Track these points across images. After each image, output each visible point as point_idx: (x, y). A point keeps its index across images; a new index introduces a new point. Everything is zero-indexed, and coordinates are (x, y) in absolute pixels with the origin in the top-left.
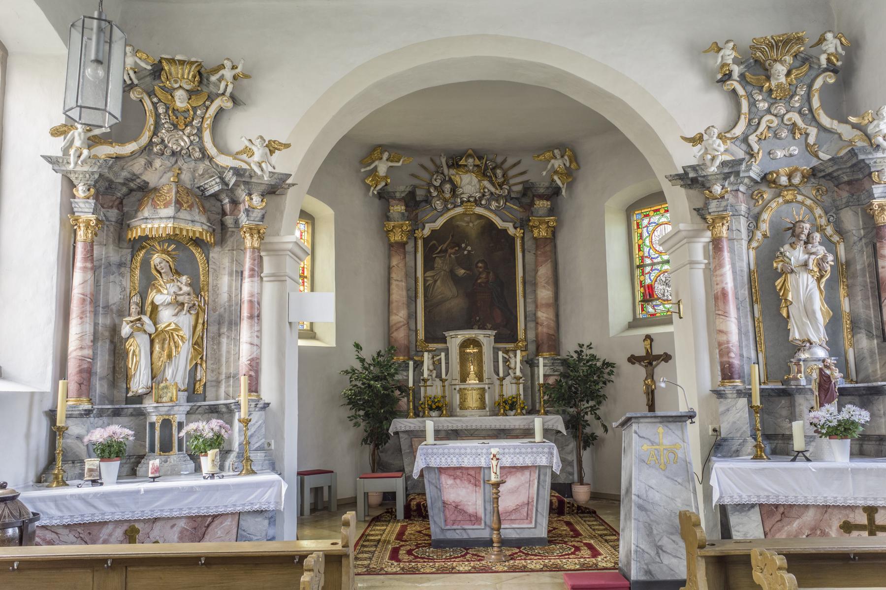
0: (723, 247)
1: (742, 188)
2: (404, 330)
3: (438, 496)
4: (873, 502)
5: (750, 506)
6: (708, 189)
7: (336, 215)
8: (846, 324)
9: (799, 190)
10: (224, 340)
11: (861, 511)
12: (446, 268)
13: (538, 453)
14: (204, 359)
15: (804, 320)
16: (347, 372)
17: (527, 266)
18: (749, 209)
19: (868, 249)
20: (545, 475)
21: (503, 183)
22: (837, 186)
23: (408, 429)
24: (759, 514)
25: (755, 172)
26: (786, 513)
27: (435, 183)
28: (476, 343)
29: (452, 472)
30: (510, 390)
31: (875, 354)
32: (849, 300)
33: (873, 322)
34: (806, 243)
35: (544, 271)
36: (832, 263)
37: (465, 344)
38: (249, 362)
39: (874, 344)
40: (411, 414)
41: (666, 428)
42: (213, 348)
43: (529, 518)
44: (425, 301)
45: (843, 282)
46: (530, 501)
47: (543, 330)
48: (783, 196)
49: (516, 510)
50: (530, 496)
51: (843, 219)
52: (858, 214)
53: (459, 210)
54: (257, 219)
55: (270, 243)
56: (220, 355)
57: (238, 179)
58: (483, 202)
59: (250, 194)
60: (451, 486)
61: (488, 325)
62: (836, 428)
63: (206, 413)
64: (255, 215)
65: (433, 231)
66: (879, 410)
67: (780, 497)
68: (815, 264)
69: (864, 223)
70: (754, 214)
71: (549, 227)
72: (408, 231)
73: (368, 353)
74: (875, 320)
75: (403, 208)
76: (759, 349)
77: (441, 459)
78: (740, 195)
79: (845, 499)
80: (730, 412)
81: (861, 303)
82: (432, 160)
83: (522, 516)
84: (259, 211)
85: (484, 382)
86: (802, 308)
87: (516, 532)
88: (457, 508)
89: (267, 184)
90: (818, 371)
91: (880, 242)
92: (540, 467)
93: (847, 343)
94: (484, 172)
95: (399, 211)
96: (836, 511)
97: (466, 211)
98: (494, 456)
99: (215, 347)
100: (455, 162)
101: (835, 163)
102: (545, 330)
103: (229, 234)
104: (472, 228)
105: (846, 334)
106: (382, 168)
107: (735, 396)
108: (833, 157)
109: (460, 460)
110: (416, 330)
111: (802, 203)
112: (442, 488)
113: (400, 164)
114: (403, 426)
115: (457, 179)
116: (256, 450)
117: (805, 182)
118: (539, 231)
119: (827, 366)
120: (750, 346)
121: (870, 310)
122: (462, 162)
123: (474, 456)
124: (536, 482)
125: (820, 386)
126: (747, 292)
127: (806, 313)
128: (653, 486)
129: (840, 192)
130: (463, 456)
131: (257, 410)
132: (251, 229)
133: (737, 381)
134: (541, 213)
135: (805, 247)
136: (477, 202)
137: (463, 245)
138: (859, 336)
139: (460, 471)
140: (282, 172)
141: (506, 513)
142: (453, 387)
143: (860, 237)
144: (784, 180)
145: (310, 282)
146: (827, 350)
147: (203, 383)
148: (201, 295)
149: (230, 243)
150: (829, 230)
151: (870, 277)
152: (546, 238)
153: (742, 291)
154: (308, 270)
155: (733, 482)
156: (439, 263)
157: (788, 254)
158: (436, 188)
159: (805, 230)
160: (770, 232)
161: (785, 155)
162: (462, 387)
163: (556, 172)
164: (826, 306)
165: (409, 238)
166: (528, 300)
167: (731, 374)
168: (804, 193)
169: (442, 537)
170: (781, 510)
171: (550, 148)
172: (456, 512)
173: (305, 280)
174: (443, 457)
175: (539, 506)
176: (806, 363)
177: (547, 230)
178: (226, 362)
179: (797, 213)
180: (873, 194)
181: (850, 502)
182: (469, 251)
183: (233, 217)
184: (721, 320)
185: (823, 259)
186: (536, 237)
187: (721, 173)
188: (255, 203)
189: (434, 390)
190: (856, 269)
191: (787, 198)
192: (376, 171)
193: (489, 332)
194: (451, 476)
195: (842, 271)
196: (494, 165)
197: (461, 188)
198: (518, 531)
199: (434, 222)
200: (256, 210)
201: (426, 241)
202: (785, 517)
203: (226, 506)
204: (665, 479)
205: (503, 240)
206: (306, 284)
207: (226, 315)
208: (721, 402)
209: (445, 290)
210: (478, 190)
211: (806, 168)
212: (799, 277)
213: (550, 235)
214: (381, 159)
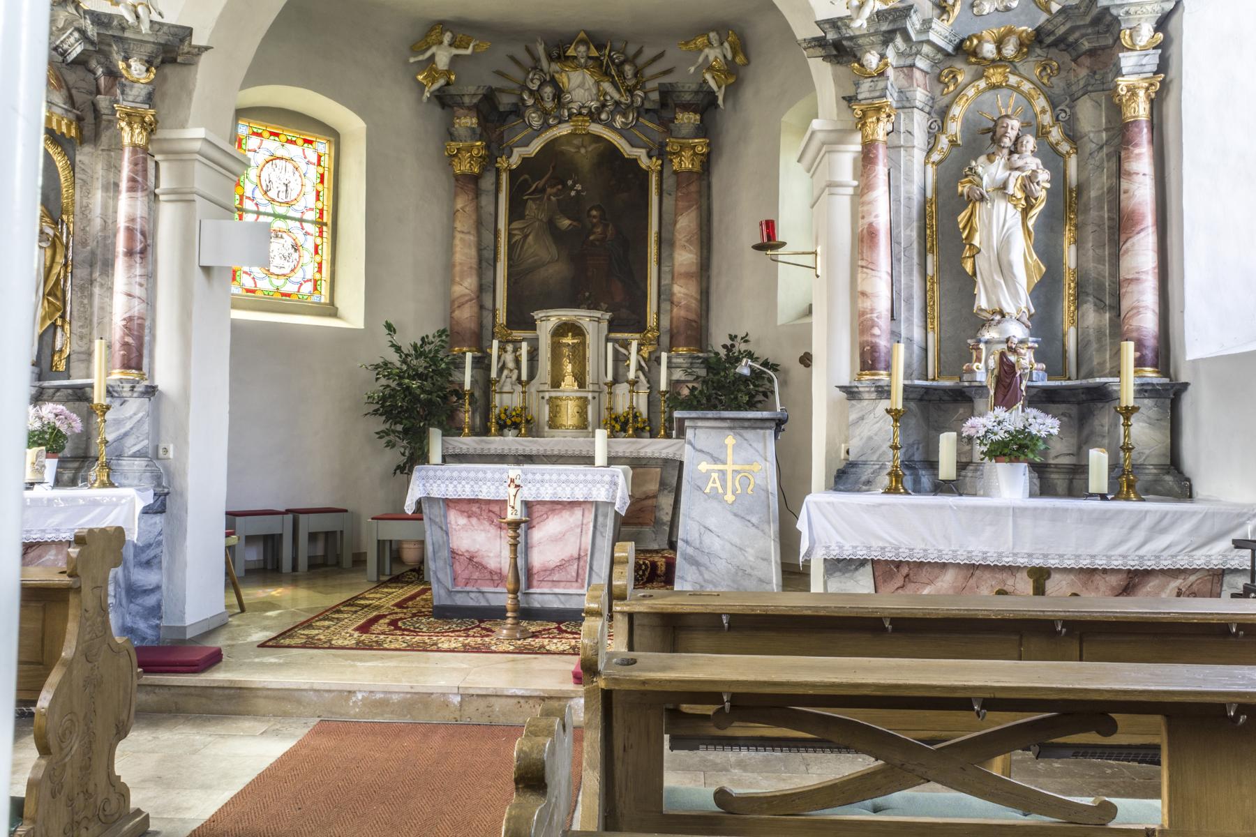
0: (876, 157)
1: (921, 63)
2: (471, 307)
3: (444, 542)
4: (1042, 561)
5: (857, 564)
6: (859, 61)
7: (368, 130)
8: (1069, 288)
9: (1015, 67)
10: (97, 290)
11: (1025, 574)
12: (542, 216)
13: (594, 482)
14: (68, 318)
15: (996, 277)
16: (377, 367)
17: (665, 216)
18: (933, 99)
19: (1110, 164)
20: (606, 516)
21: (635, 87)
22: (1075, 60)
23: (457, 451)
24: (872, 576)
25: (941, 33)
26: (911, 575)
27: (531, 86)
28: (577, 330)
29: (465, 507)
30: (623, 401)
31: (1106, 335)
32: (1078, 250)
33: (1107, 284)
34: (1011, 153)
35: (686, 223)
36: (1048, 185)
37: (562, 330)
38: (124, 323)
39: (1106, 320)
40: (466, 430)
41: (738, 437)
42: (82, 303)
43: (579, 580)
44: (509, 267)
45: (1070, 219)
46: (582, 554)
47: (679, 313)
48: (987, 77)
49: (561, 567)
50: (583, 547)
51: (1080, 116)
52: (1100, 106)
53: (565, 130)
54: (139, 99)
55: (165, 140)
56: (92, 314)
57: (101, 32)
58: (603, 116)
59: (126, 59)
60: (464, 527)
61: (602, 304)
62: (1003, 444)
63: (69, 401)
64: (135, 92)
65: (525, 161)
66: (1102, 426)
67: (900, 550)
68: (1018, 185)
69: (1109, 121)
70: (941, 108)
71: (695, 154)
72: (480, 157)
73: (408, 339)
74: (1110, 281)
75: (474, 120)
76: (929, 326)
77: (447, 486)
78: (917, 74)
79: (1000, 555)
80: (865, 421)
81: (1091, 252)
82: (528, 50)
83: (569, 577)
84: (142, 86)
85: (587, 389)
86: (993, 258)
87: (560, 600)
88: (472, 560)
89: (154, 43)
90: (997, 357)
91: (1125, 149)
92: (596, 504)
93: (1066, 318)
94: (602, 69)
95: (469, 125)
96: (987, 575)
97: (576, 130)
98: (512, 481)
99: (86, 301)
100: (562, 53)
101: (1068, 18)
102: (683, 313)
103: (104, 124)
104: (585, 156)
105: (1067, 305)
106: (442, 57)
107: (874, 395)
108: (1064, 7)
109: (476, 489)
110: (494, 310)
111: (1016, 89)
112: (450, 530)
113: (469, 51)
114: (450, 447)
115: (563, 79)
116: (134, 456)
117: (1024, 54)
118: (681, 160)
119: (1011, 348)
120: (913, 321)
121: (1104, 265)
122: (571, 52)
123: (497, 484)
124: (591, 525)
125: (999, 381)
126: (915, 234)
127: (1000, 267)
128: (712, 527)
129: (1079, 70)
130: (480, 483)
131: (135, 395)
132: (128, 115)
133: (882, 372)
134: (684, 131)
135: (1009, 159)
136: (594, 116)
137: (570, 182)
138: (1085, 306)
139: (477, 505)
140: (174, 23)
141: (545, 570)
142: (541, 395)
143: (1101, 143)
144: (989, 50)
145: (330, 232)
146: (1027, 327)
147: (65, 355)
148: (62, 221)
149: (105, 138)
150: (1056, 134)
151: (1109, 211)
152: (690, 172)
153: (908, 232)
154: (328, 213)
155: (832, 525)
156: (532, 208)
157: (980, 170)
158: (532, 93)
159: (1009, 130)
160: (963, 136)
161: (996, 9)
162: (553, 394)
163: (710, 68)
164: (1035, 257)
165: (484, 169)
166: (664, 269)
167: (872, 361)
168: (1022, 72)
169: (448, 602)
170: (905, 570)
171: (703, 30)
172: (470, 566)
173: (325, 228)
174: (451, 483)
175: (595, 563)
176: (989, 345)
177: (693, 160)
178: (99, 324)
179: (1004, 102)
180: (1121, 69)
181: (1007, 560)
182: (578, 192)
183: (108, 97)
184: (865, 275)
185: (1032, 178)
186: (675, 171)
187: (876, 33)
188: (135, 72)
189: (507, 399)
190: (1089, 197)
191: (993, 80)
192: (434, 63)
193: (598, 314)
194: (464, 512)
195: (1070, 202)
196: (622, 58)
197: (570, 93)
198: (562, 598)
199: (527, 145)
200: (136, 85)
201: (513, 174)
202: (910, 581)
203: (44, 531)
204: (731, 517)
205: (630, 176)
206: (325, 234)
207: (99, 252)
208: (853, 406)
209: (539, 249)
210: (595, 97)
211: (1026, 29)
212: (993, 206)
213: (697, 168)
214: (441, 43)
